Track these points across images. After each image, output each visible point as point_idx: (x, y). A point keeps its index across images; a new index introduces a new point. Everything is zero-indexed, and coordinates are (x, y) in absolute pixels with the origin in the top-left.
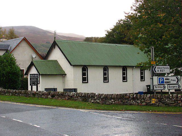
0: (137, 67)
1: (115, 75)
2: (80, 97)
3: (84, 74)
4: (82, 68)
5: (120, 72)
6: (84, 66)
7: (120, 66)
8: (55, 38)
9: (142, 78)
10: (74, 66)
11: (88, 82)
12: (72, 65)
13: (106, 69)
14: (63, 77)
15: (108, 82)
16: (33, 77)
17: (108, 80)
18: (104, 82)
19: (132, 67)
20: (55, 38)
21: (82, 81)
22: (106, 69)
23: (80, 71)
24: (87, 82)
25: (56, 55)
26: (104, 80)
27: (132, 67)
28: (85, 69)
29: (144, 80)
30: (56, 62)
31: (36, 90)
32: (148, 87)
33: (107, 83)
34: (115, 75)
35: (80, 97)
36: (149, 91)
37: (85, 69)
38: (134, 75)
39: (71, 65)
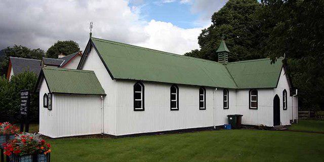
0: (219, 89)
1: (188, 98)
3: (137, 96)
4: (134, 86)
5: (196, 94)
6: (138, 82)
8: (91, 34)
9: (226, 105)
10: (119, 80)
11: (143, 110)
12: (115, 79)
13: (174, 88)
14: (101, 99)
15: (205, 109)
16: (303, 115)
17: (178, 107)
18: (171, 110)
19: (213, 88)
20: (91, 34)
21: (133, 108)
22: (174, 88)
23: (130, 89)
24: (142, 108)
25: (93, 63)
28: (139, 86)
29: (228, 108)
30: (92, 73)
31: (270, 123)
32: (231, 118)
33: (142, 112)
34: (188, 98)
36: (235, 122)
37: (139, 86)
38: (214, 99)
39: (113, 78)
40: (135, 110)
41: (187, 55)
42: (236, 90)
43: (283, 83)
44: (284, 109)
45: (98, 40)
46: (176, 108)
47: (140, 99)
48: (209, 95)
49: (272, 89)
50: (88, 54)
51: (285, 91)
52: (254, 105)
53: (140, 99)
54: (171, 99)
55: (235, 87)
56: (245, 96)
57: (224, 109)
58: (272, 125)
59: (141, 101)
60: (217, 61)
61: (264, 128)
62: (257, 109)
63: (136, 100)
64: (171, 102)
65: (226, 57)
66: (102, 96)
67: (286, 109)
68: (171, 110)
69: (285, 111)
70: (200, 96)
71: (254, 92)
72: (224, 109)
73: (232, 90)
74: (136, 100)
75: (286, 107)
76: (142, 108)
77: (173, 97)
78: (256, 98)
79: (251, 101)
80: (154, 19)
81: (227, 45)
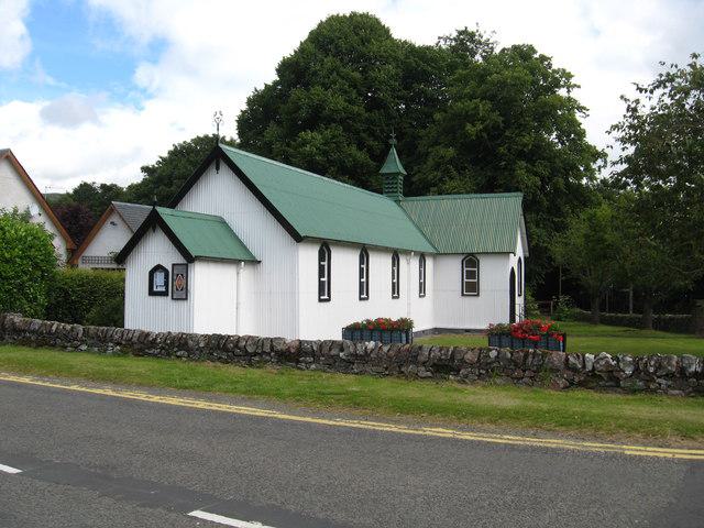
2: (669, 376)
19: (407, 252)
35: (669, 376)
43: (520, 252)
48: (403, 261)
52: (471, 288)
56: (453, 270)
57: (320, 300)
62: (478, 295)
66: (254, 262)
67: (398, 297)
71: (471, 262)
72: (320, 300)
78: (471, 275)
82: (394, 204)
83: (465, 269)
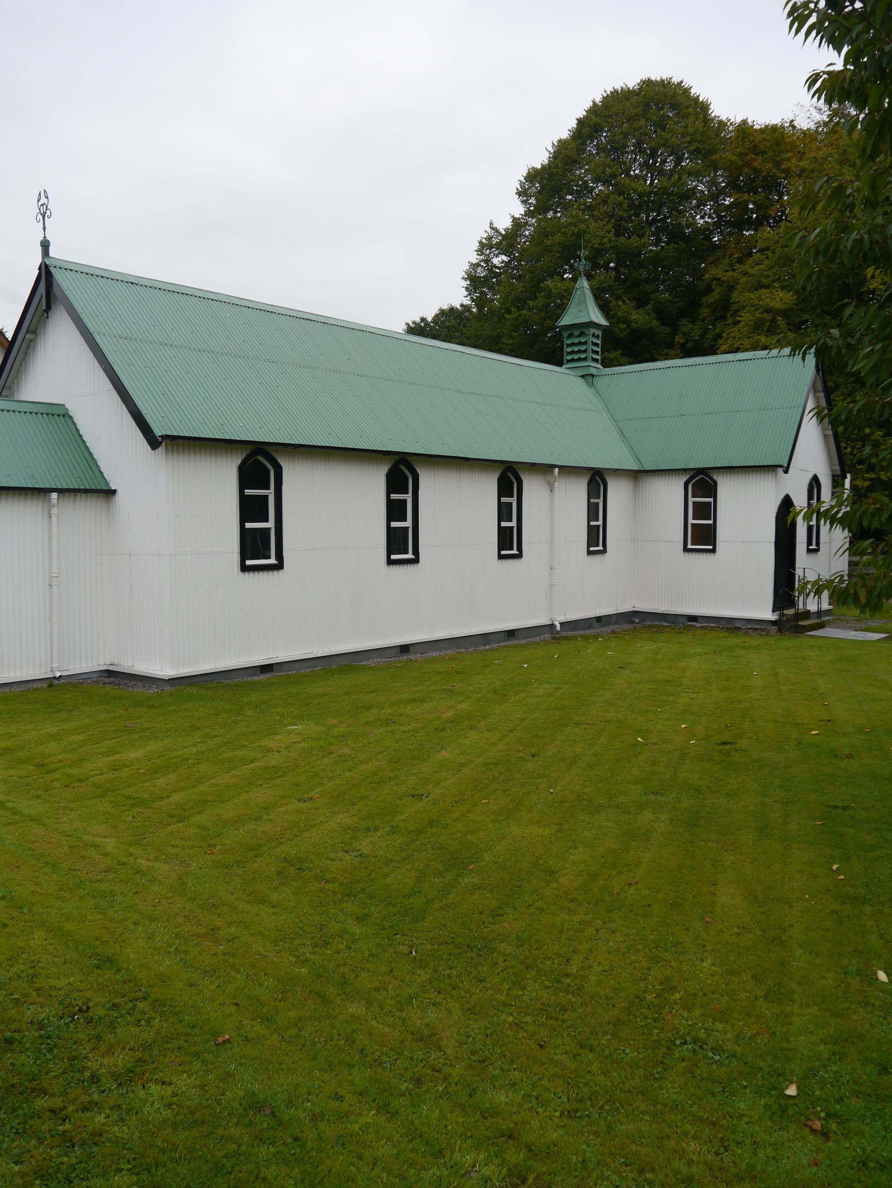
0: (568, 470)
7: (568, 470)
8: (45, 246)
17: (416, 551)
18: (390, 562)
20: (45, 246)
26: (501, 547)
27: (543, 469)
33: (712, 554)
39: (153, 441)
40: (244, 568)
41: (419, 329)
42: (637, 475)
44: (809, 551)
45: (71, 269)
46: (515, 552)
47: (694, 503)
49: (770, 468)
50: (35, 332)
51: (815, 483)
53: (694, 503)
54: (390, 518)
55: (635, 467)
57: (590, 553)
58: (768, 614)
59: (512, 528)
60: (560, 364)
61: (730, 626)
62: (713, 551)
63: (248, 525)
64: (500, 528)
65: (594, 340)
67: (817, 551)
68: (390, 562)
69: (813, 556)
70: (500, 504)
72: (590, 553)
73: (617, 472)
74: (248, 525)
75: (818, 544)
76: (600, 548)
77: (395, 511)
78: (705, 511)
79: (691, 521)
80: (806, 133)
81: (597, 296)
82: (581, 380)
83: (691, 500)
